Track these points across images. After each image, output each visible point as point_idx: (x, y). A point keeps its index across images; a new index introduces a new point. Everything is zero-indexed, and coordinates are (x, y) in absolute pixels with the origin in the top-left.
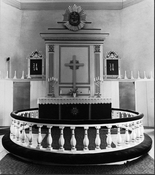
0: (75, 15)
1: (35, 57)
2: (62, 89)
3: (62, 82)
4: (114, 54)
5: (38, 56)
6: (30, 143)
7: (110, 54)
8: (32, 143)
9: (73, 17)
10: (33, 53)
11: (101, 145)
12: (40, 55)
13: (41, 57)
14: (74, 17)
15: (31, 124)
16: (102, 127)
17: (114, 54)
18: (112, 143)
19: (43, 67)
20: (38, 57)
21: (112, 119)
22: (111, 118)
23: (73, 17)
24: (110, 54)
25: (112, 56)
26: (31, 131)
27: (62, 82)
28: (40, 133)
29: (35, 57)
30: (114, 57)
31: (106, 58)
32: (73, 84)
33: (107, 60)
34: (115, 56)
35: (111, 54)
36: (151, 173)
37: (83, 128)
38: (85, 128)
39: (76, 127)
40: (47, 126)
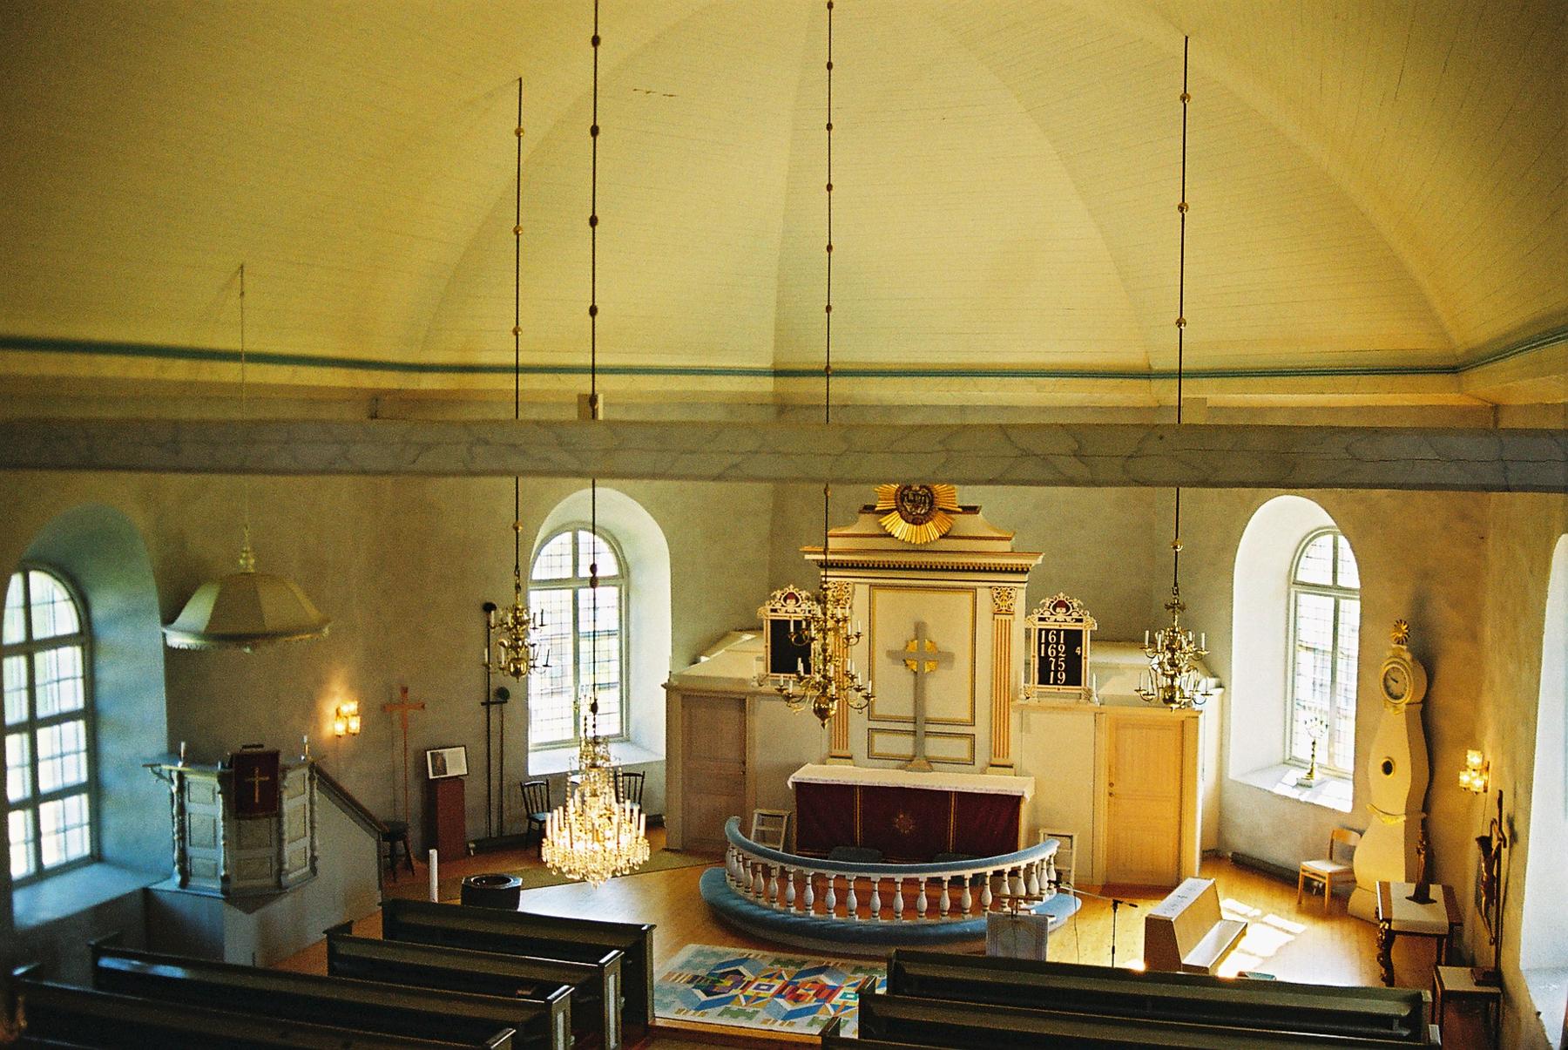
0: (916, 491)
1: (1055, 621)
2: (877, 737)
4: (1068, 609)
5: (798, 610)
7: (1054, 609)
9: (911, 497)
10: (1048, 605)
11: (991, 905)
12: (1075, 615)
14: (914, 495)
17: (1068, 609)
21: (519, 910)
22: (517, 905)
23: (911, 497)
24: (1054, 609)
25: (1060, 617)
29: (1055, 621)
30: (1068, 619)
32: (928, 734)
33: (772, 672)
35: (1058, 610)
36: (649, 1023)
37: (917, 879)
38: (920, 880)
39: (928, 878)
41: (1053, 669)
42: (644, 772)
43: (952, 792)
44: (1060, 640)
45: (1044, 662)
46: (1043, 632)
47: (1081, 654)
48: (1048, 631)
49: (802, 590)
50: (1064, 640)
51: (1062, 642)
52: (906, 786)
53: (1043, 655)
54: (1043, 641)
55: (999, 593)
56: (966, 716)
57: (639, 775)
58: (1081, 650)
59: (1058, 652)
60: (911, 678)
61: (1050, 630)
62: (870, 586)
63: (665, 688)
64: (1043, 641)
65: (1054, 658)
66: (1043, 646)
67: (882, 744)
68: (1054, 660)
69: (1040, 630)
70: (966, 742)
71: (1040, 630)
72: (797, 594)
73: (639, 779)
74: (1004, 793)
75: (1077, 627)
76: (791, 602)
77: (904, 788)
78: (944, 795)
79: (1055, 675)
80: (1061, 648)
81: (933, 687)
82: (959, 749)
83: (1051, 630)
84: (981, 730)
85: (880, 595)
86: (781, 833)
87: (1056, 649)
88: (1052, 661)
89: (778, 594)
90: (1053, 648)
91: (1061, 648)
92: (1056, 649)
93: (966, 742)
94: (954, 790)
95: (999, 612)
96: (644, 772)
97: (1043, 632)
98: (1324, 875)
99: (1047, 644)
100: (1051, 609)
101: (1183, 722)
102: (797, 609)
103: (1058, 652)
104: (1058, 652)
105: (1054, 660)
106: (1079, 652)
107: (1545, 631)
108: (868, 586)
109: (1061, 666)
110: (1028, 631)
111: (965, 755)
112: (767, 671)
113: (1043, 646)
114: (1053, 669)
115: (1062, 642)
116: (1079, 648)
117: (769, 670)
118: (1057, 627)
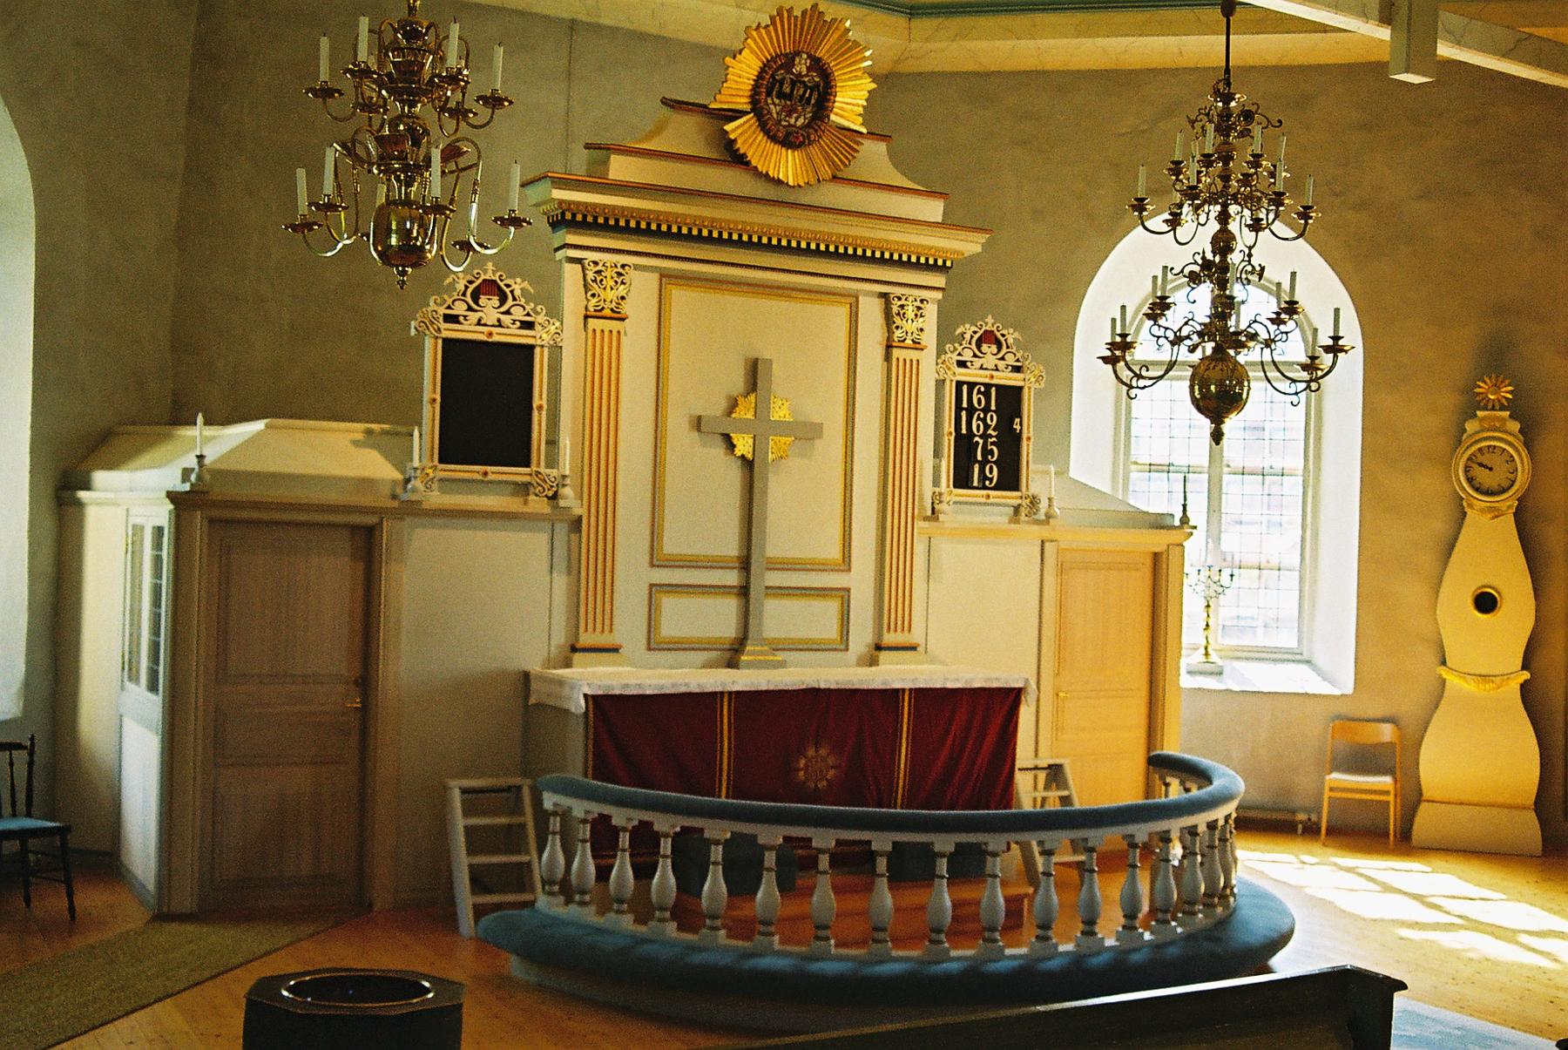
2: (668, 603)
3: (670, 547)
4: (503, 300)
5: (506, 319)
6: (1087, 928)
7: (475, 298)
8: (1050, 933)
10: (967, 336)
13: (1017, 369)
15: (630, 819)
16: (685, 830)
18: (1039, 927)
19: (540, 407)
20: (500, 324)
24: (475, 298)
25: (990, 361)
26: (665, 857)
27: (670, 547)
28: (883, 883)
31: (443, 325)
34: (1003, 359)
35: (985, 347)
37: (927, 846)
40: (932, 843)
41: (979, 458)
42: (32, 739)
43: (903, 690)
44: (990, 406)
45: (964, 446)
46: (965, 388)
47: (1021, 430)
48: (971, 385)
49: (513, 277)
50: (997, 405)
51: (993, 408)
52: (823, 686)
53: (964, 431)
54: (965, 405)
55: (599, 272)
56: (834, 553)
57: (19, 746)
58: (1021, 425)
59: (985, 426)
60: (733, 476)
61: (976, 384)
62: (662, 276)
63: (172, 501)
64: (965, 405)
65: (980, 437)
66: (964, 414)
67: (680, 617)
68: (981, 441)
69: (959, 384)
70: (832, 607)
71: (959, 384)
72: (998, 334)
73: (21, 757)
74: (994, 685)
75: (1012, 380)
76: (489, 303)
77: (818, 690)
78: (893, 695)
79: (982, 471)
80: (992, 420)
81: (778, 492)
82: (820, 619)
83: (976, 384)
84: (860, 581)
85: (680, 297)
86: (523, 826)
87: (984, 420)
88: (977, 443)
89: (968, 329)
90: (979, 418)
91: (992, 420)
92: (984, 420)
93: (832, 607)
94: (908, 686)
95: (599, 314)
96: (32, 739)
97: (965, 388)
98: (1386, 789)
99: (971, 410)
100: (974, 346)
101: (1156, 557)
102: (503, 317)
103: (987, 427)
104: (987, 427)
105: (981, 441)
106: (1018, 427)
107: (30, 417)
108: (656, 276)
109: (992, 452)
110: (940, 384)
111: (831, 632)
112: (432, 461)
113: (964, 414)
114: (979, 458)
115: (993, 408)
116: (1017, 420)
117: (436, 456)
118: (987, 381)
